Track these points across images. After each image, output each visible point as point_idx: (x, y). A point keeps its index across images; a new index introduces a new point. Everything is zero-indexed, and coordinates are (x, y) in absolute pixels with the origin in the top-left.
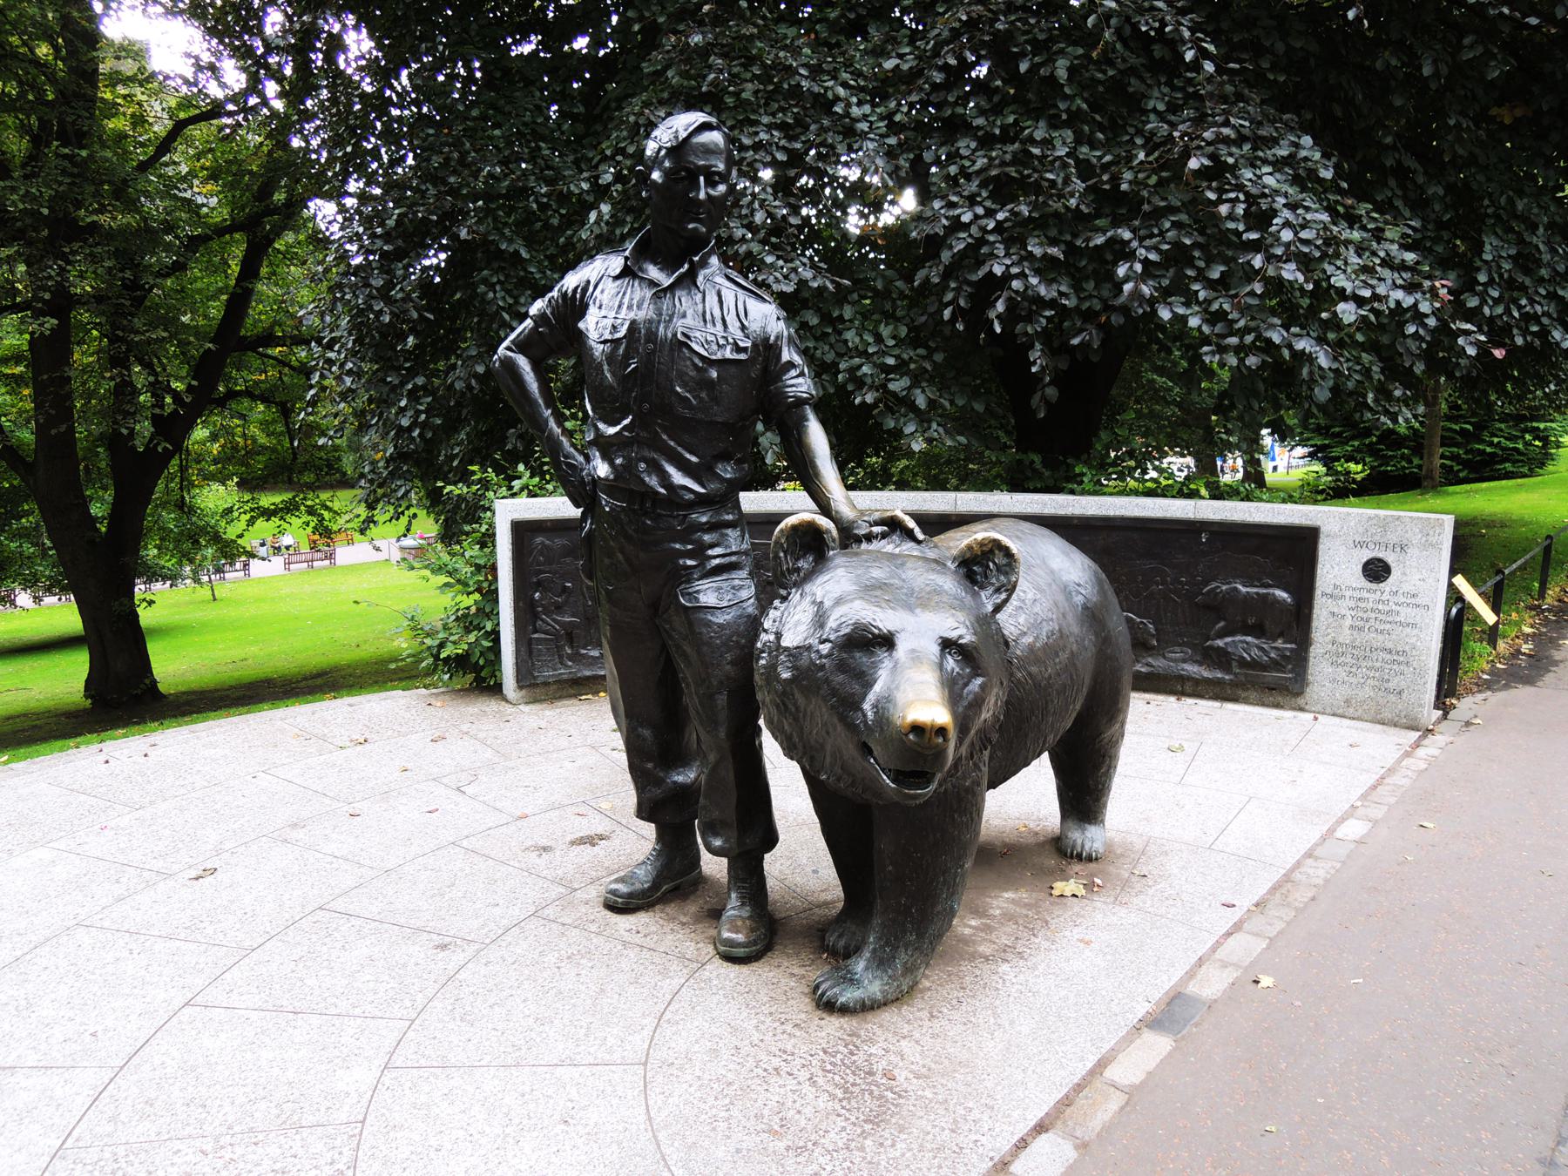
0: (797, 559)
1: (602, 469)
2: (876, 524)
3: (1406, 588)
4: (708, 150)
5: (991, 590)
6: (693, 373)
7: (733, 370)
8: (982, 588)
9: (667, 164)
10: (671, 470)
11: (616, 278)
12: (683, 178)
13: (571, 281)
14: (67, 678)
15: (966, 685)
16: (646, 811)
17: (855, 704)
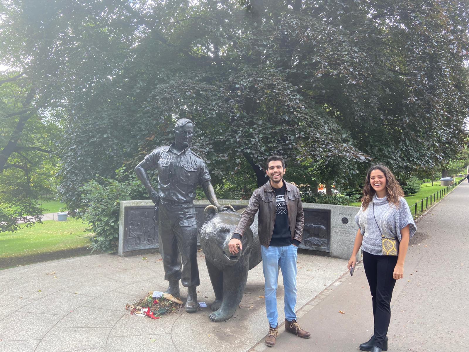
1: (162, 195)
2: (225, 207)
4: (189, 127)
7: (193, 173)
9: (180, 130)
10: (179, 195)
11: (167, 152)
13: (155, 151)
17: (221, 243)
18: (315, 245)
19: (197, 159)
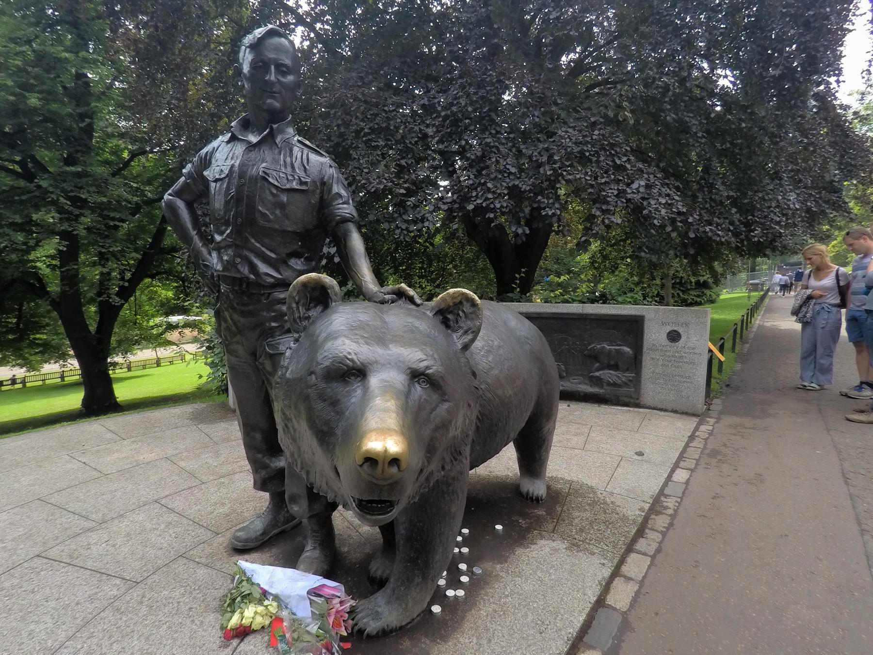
0: (308, 309)
3: (690, 345)
5: (461, 332)
6: (270, 198)
7: (297, 196)
8: (455, 331)
12: (260, 67)
14: (74, 400)
15: (433, 410)
16: (262, 485)
18: (609, 384)
19: (313, 157)
